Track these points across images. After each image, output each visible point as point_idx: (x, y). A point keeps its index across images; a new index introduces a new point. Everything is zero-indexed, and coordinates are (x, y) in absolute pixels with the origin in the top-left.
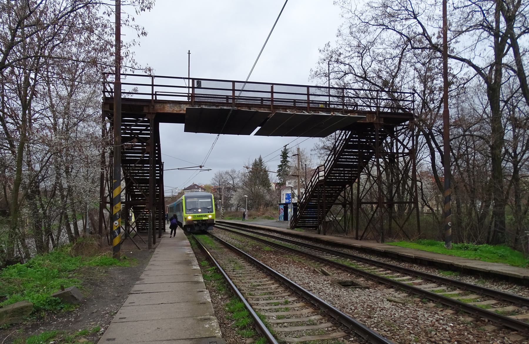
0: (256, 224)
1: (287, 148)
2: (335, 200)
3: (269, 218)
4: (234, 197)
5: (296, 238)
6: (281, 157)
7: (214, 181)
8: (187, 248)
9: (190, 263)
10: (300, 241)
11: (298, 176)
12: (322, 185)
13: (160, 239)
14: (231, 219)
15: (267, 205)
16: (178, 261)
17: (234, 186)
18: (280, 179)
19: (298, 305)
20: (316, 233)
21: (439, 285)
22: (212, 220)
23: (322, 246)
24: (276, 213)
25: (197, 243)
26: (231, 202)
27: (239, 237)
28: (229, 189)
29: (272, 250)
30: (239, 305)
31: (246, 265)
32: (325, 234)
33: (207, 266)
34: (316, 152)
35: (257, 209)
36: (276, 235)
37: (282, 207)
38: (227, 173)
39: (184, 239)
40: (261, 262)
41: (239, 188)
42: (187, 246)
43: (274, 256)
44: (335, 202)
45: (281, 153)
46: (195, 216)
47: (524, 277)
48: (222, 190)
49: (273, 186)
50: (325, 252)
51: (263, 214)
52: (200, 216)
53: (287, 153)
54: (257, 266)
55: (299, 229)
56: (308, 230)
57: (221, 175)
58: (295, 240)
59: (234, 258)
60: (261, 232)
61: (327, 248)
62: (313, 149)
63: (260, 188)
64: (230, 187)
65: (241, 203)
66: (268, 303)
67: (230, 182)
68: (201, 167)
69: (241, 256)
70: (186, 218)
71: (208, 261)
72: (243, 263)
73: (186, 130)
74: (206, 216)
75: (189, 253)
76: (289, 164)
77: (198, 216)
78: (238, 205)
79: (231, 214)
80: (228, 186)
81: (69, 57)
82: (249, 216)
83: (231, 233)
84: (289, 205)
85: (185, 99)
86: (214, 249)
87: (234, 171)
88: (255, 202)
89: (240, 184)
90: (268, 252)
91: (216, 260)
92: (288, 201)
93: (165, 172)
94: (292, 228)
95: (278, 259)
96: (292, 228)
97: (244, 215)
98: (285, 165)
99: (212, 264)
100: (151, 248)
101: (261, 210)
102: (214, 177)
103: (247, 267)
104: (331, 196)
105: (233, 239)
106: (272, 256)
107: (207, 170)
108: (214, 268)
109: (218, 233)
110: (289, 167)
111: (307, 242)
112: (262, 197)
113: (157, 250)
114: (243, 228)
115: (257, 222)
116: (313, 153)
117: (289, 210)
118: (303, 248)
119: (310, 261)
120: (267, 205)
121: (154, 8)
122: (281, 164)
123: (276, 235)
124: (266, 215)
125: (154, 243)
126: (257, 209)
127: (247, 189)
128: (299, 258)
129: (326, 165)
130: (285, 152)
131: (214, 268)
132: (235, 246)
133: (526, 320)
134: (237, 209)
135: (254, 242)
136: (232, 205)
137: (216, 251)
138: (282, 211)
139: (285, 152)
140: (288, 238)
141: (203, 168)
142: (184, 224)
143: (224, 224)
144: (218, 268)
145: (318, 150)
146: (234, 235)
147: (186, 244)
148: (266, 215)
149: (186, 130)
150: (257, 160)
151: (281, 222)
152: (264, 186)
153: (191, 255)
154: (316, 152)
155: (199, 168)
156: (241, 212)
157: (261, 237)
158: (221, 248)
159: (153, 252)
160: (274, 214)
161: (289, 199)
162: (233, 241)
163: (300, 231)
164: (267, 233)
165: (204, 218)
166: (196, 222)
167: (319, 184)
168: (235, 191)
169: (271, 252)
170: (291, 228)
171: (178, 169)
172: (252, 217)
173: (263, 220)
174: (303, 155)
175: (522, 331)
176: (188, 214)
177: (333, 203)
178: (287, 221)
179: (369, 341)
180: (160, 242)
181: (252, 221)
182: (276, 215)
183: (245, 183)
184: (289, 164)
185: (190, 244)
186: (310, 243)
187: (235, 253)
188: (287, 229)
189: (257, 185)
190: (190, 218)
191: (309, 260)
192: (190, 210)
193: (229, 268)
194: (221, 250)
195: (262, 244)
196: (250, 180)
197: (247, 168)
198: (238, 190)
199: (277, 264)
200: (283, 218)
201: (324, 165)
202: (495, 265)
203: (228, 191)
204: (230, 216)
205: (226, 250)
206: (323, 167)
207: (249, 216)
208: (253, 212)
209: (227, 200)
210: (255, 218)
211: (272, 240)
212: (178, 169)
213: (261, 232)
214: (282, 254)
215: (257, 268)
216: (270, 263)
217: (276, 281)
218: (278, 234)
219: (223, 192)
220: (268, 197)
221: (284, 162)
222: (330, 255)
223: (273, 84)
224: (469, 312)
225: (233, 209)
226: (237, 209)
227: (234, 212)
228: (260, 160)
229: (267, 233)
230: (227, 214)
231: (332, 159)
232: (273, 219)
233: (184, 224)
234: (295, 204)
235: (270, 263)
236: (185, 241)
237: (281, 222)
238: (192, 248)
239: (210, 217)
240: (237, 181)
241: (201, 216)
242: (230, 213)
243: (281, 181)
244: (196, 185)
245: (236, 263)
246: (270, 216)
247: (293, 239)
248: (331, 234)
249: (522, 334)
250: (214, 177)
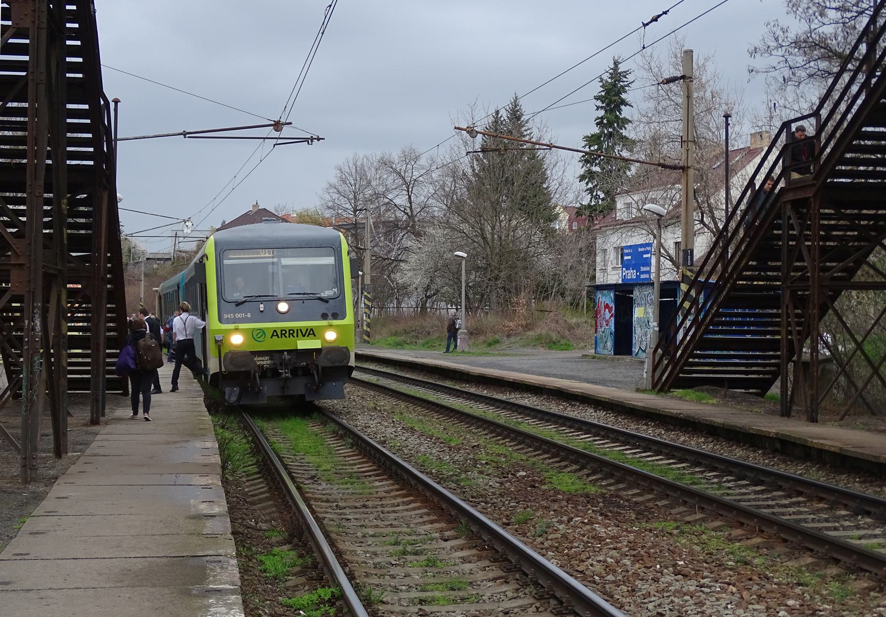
0: (501, 367)
1: (622, 68)
2: (852, 272)
3: (551, 344)
4: (413, 258)
5: (686, 432)
6: (599, 103)
7: (336, 196)
8: (203, 481)
9: (201, 575)
11: (684, 169)
12: (804, 202)
13: (95, 428)
14: (399, 345)
15: (542, 291)
16: (139, 564)
17: (411, 217)
18: (591, 191)
20: (772, 413)
22: (338, 352)
23: (816, 476)
24: (578, 325)
25: (257, 448)
26: (399, 278)
27: (436, 425)
28: (392, 228)
29: (592, 490)
31: (480, 576)
32: (813, 420)
33: (293, 581)
34: (773, 60)
35: (506, 307)
36: (591, 415)
37: (606, 299)
38: (385, 163)
39: (196, 433)
40: (552, 566)
41: (432, 221)
42: (204, 469)
43: (613, 530)
44: (856, 279)
45: (597, 89)
46: (262, 331)
47: (777, 434)
48: (368, 229)
49: (562, 224)
50: (846, 507)
51: (528, 327)
52: (284, 333)
53: (623, 89)
54: (536, 584)
55: (690, 394)
56: (733, 397)
57: (361, 173)
58: (682, 440)
59: (422, 529)
60: (528, 401)
61: (841, 486)
62: (759, 44)
63: (514, 222)
64: (397, 220)
65: (439, 281)
67: (398, 201)
68: (277, 125)
69: (451, 521)
70: (219, 344)
71: (295, 547)
72: (464, 560)
74: (310, 333)
75: (204, 508)
76: (629, 132)
77: (275, 333)
78: (428, 288)
79: (400, 327)
80: (390, 216)
82: (474, 333)
83: (403, 405)
84: (636, 294)
86: (329, 481)
87: (411, 158)
88: (497, 279)
89: (438, 209)
90: (571, 498)
91: (332, 544)
92: (632, 274)
93: (123, 151)
94: (660, 387)
95: (632, 546)
97: (453, 331)
98: (610, 135)
99: (315, 566)
100: (34, 480)
101: (521, 310)
102: (334, 181)
103: (489, 590)
104: (840, 255)
105: (412, 430)
106: (601, 530)
107: (306, 140)
108: (325, 593)
110: (629, 143)
111: (738, 454)
112: (524, 259)
113: (58, 490)
114: (448, 384)
115: (514, 361)
116: (761, 62)
117: (638, 313)
118: (729, 482)
119: (790, 556)
120: (542, 291)
122: (596, 130)
123: (591, 415)
124: (541, 330)
125: (59, 451)
126: (506, 307)
127: (465, 227)
128: (730, 540)
129: (824, 113)
130: (615, 85)
131: (325, 593)
132: (422, 467)
134: (424, 308)
135: (505, 449)
136: (403, 290)
137: (336, 490)
138: (608, 315)
139: (615, 85)
140: (648, 432)
141: (286, 132)
142: (213, 366)
143: (372, 367)
144: (343, 596)
145: (780, 52)
146: (413, 416)
147: (199, 459)
148: (541, 330)
150: (504, 114)
151: (604, 359)
152: (530, 215)
153: (211, 526)
154: (773, 60)
155: (270, 132)
156: (440, 319)
157: (529, 426)
158: (358, 476)
159: (38, 498)
160: (570, 328)
161: (636, 267)
162: (413, 441)
163: (699, 401)
164: (554, 408)
165: (303, 344)
166: (265, 362)
167: (791, 196)
168: (418, 235)
169: (590, 499)
170: (654, 386)
171: (184, 134)
172: (482, 338)
173: (529, 350)
174: (702, 86)
176: (228, 321)
177: (847, 282)
178: (627, 358)
180: (87, 444)
181: (486, 354)
182: (578, 332)
183: (456, 207)
184: (629, 132)
185: (217, 459)
186: (755, 459)
187: (425, 501)
188: (638, 390)
189: (504, 211)
190: (237, 340)
191: (780, 549)
192: (238, 304)
193: (396, 590)
194: (358, 488)
195: (540, 460)
196: (477, 190)
197: (472, 132)
198: (430, 230)
199: (636, 574)
200: (610, 344)
201: (816, 114)
202: (534, 380)
203: (386, 234)
204: (396, 334)
205: (382, 486)
206: (813, 120)
207: (474, 333)
208: (491, 320)
209: (383, 271)
210: (497, 342)
211: (579, 442)
212: (184, 134)
213: (528, 401)
214: (644, 513)
215: (540, 598)
216: (598, 568)
218: (602, 414)
219: (367, 237)
220: (546, 261)
221: (610, 124)
222: (869, 527)
225: (409, 304)
226: (424, 308)
227: (413, 318)
228: (516, 114)
229: (554, 408)
230: (384, 325)
231: (855, 89)
232: (567, 347)
233: (213, 366)
234: (668, 289)
235: (598, 568)
236: (198, 444)
237: (604, 359)
238: (225, 482)
239: (331, 336)
240: (423, 194)
241: (292, 333)
242: (395, 320)
243: (597, 197)
245: (431, 563)
246: (554, 336)
247: (672, 435)
248: (843, 417)
250: (334, 181)
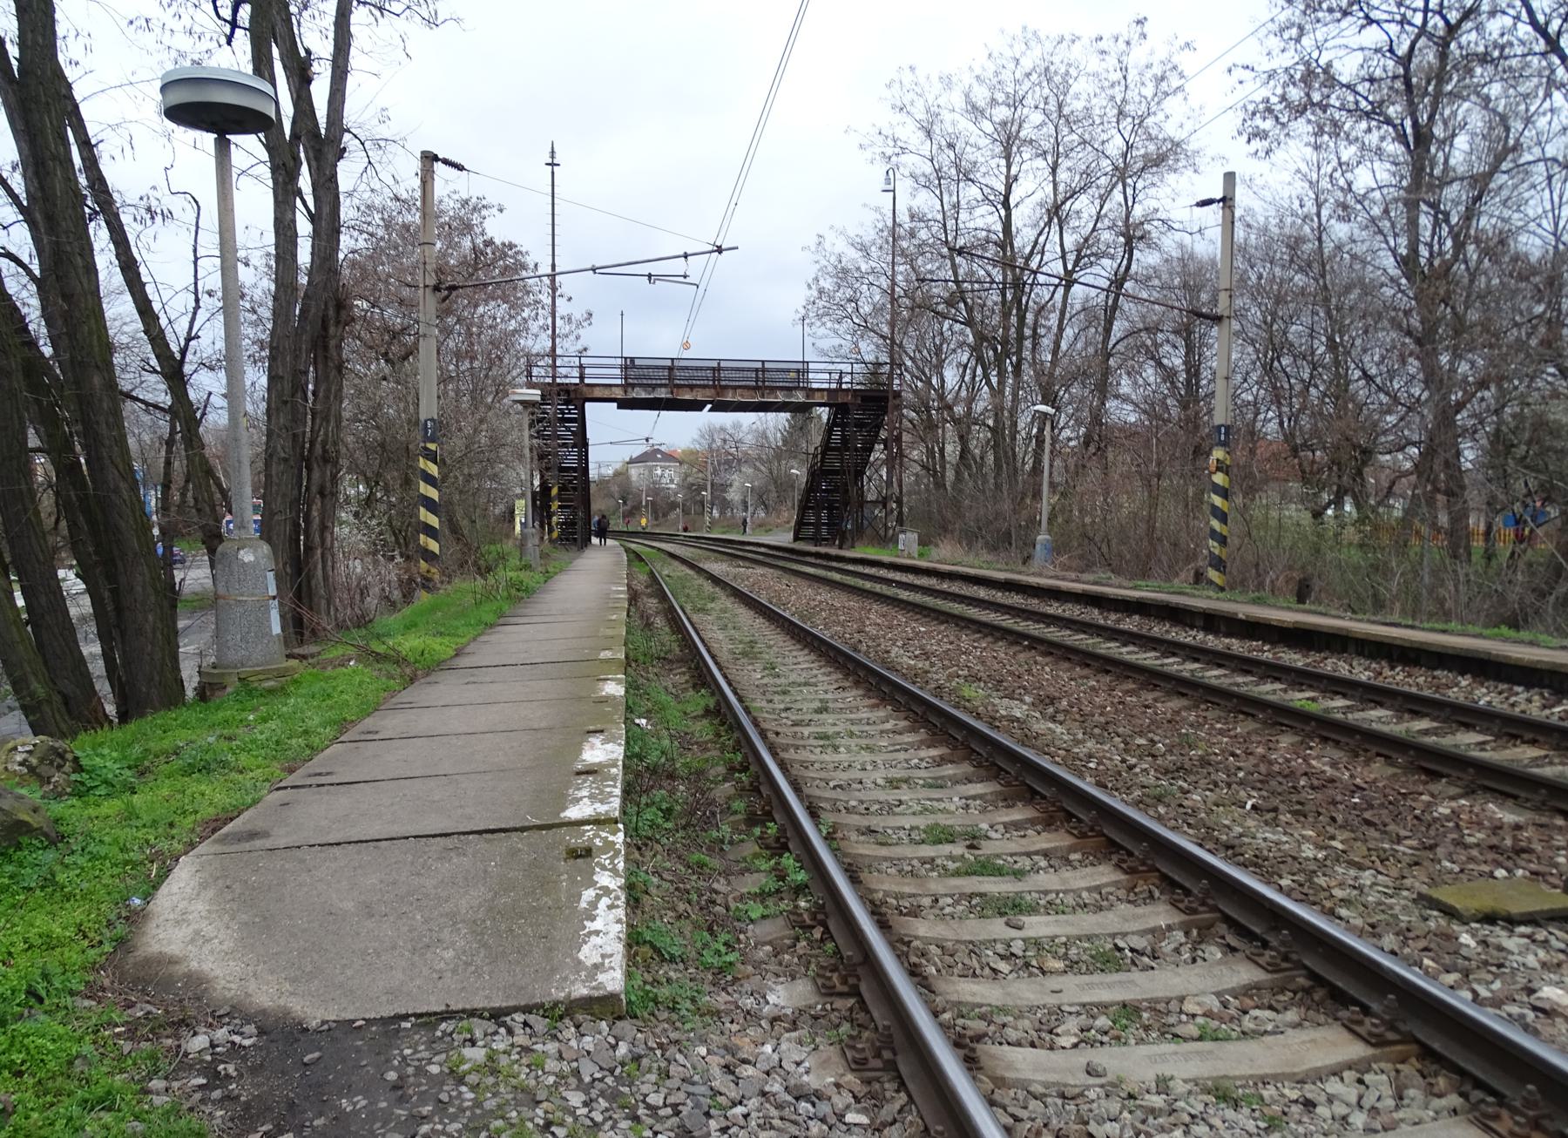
10: (781, 554)
19: (934, 752)
21: (1048, 626)
30: (267, 88)
66: (1129, 1010)
73: (619, 408)
81: (741, 791)
85: (619, 382)
96: (796, 539)
102: (696, 437)
109: (707, 558)
121: (592, 310)
123: (763, 550)
133: (1562, 774)
149: (619, 408)
157: (750, 555)
175: (1529, 796)
179: (1149, 862)
187: (782, 627)
217: (883, 699)
223: (894, 191)
224: (1295, 724)
244: (659, 451)
249: (1528, 805)
250: (696, 437)
